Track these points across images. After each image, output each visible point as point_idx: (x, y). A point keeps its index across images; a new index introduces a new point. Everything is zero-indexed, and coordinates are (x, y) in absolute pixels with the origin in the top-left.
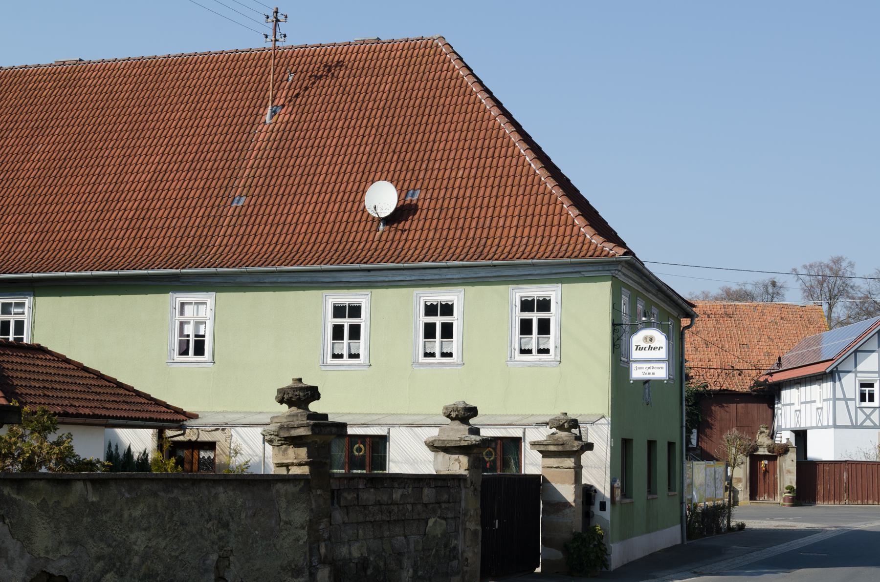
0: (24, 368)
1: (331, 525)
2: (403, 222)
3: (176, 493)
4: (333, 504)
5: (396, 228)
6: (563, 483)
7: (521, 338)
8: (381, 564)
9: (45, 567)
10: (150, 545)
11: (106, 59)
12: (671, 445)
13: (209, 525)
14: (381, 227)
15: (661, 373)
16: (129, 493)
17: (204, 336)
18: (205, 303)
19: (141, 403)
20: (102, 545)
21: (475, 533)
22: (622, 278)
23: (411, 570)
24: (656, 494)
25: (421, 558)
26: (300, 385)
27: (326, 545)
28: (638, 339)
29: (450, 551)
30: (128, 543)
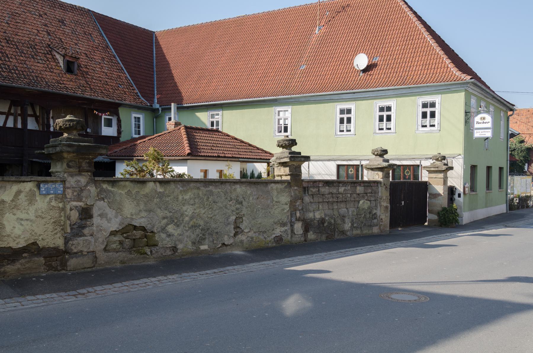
0: (206, 138)
1: (303, 203)
2: (370, 71)
3: (211, 188)
4: (305, 193)
5: (367, 74)
6: (438, 184)
7: (422, 120)
8: (333, 221)
9: (131, 222)
10: (195, 212)
11: (255, 13)
12: (501, 169)
13: (231, 203)
14: (361, 74)
15: (488, 134)
16: (182, 188)
17: (287, 124)
18: (287, 111)
19: (258, 152)
20: (166, 212)
21: (386, 207)
22: (471, 91)
23: (350, 224)
24: (491, 190)
25: (356, 219)
26: (287, 139)
27: (300, 213)
28: (477, 119)
29: (372, 215)
30: (182, 211)
